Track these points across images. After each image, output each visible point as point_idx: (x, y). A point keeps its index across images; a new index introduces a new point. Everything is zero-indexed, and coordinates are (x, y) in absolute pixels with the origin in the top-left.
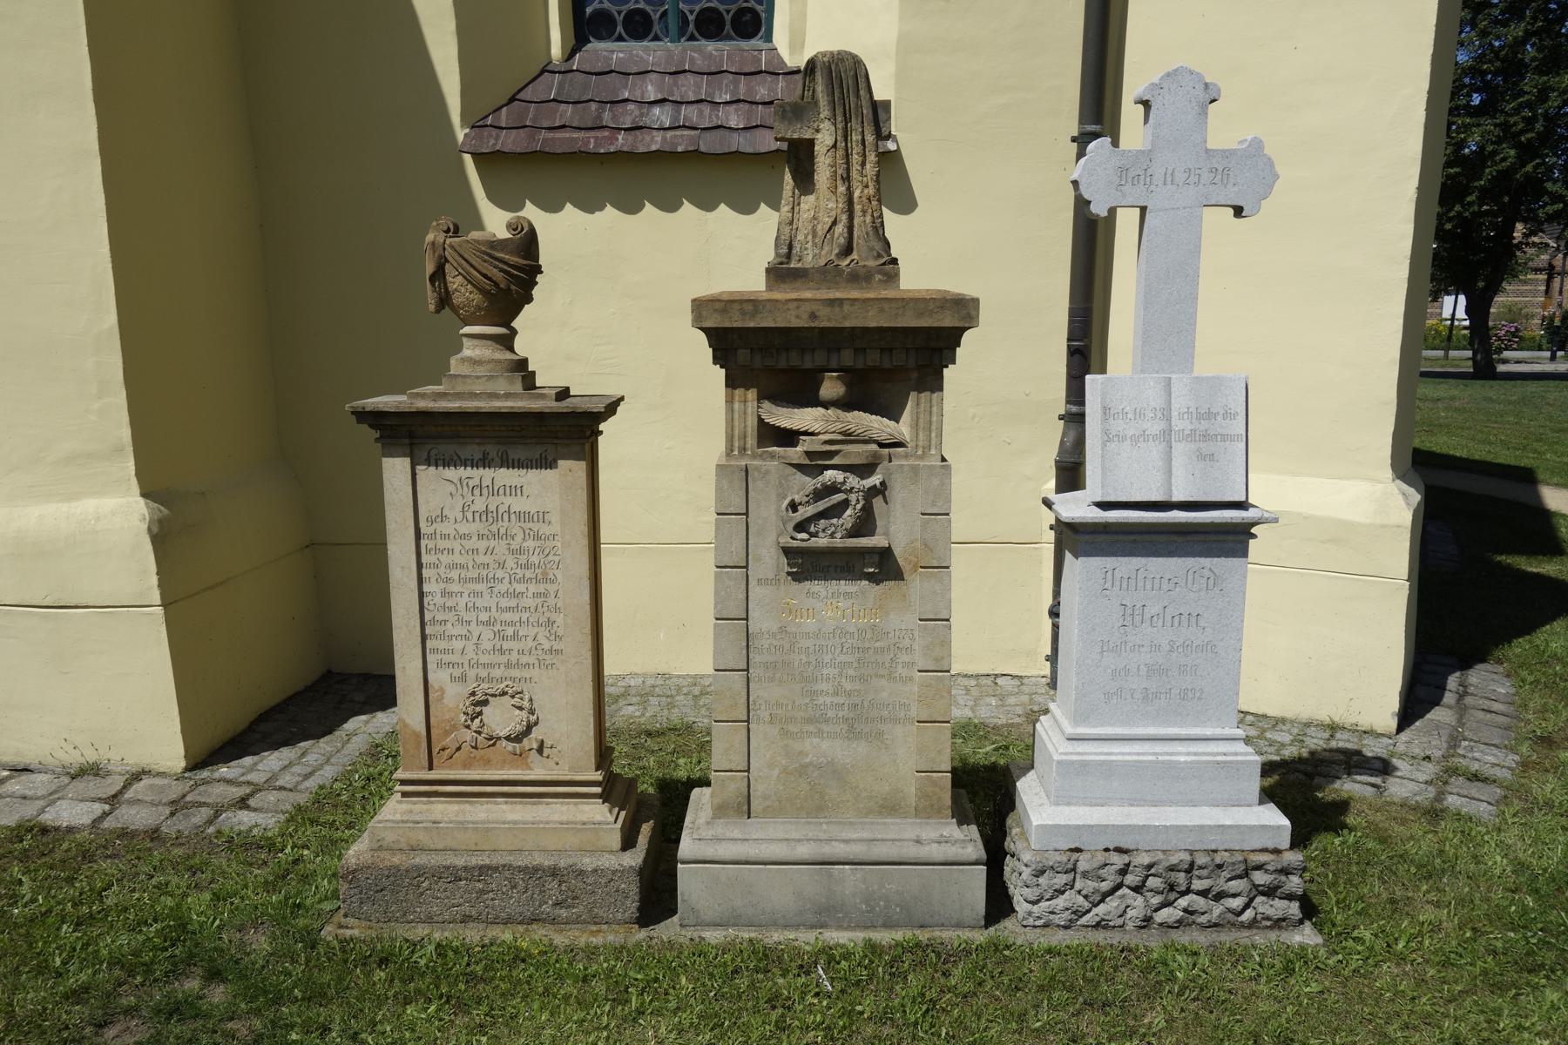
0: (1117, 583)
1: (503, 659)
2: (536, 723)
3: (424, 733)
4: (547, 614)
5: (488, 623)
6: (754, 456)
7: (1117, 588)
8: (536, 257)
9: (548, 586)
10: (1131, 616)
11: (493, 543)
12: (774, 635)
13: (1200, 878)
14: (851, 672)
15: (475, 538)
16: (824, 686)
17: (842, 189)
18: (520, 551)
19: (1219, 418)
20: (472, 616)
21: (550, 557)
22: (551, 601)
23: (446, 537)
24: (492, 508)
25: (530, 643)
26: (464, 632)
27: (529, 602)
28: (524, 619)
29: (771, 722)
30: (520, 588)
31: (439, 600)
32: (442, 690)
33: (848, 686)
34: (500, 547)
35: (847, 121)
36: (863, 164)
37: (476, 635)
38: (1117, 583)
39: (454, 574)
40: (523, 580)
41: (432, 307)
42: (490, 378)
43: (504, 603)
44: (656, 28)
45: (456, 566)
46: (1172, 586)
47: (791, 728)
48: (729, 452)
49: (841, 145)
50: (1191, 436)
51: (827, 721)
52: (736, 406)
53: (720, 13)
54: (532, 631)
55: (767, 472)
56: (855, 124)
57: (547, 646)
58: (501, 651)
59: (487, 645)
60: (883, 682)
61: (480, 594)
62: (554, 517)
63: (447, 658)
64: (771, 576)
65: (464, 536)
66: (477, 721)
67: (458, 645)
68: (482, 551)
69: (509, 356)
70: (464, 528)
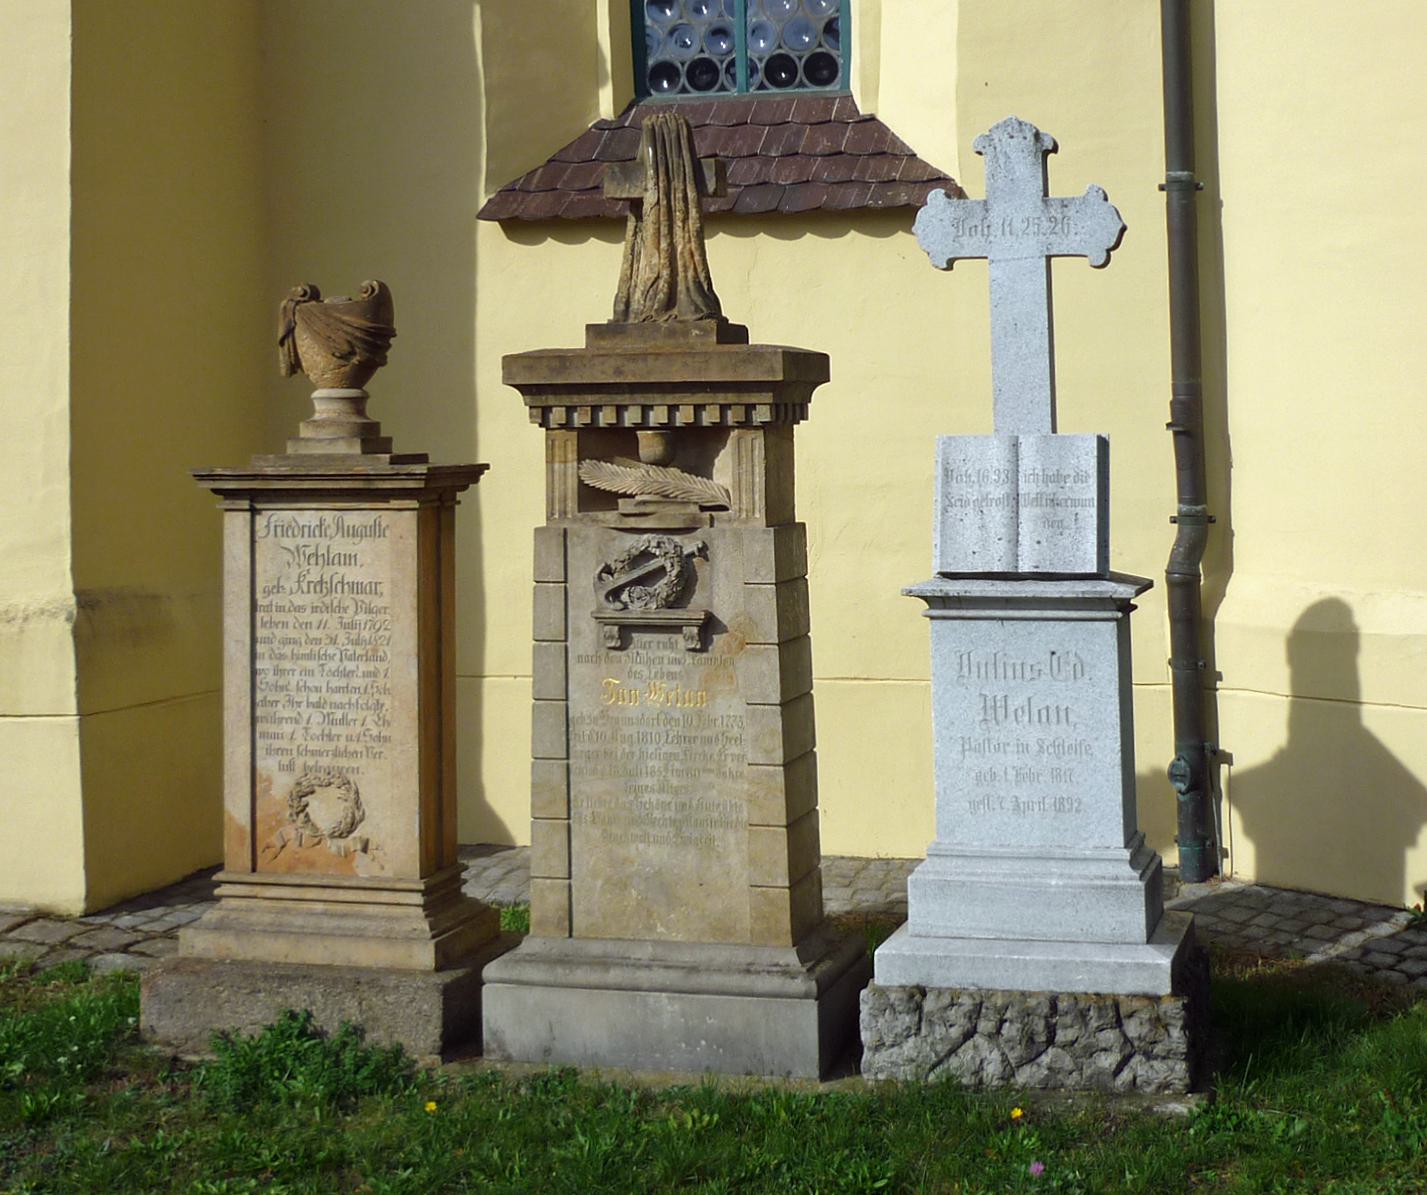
0: (974, 669)
1: (331, 746)
2: (361, 820)
3: (248, 828)
4: (376, 696)
5: (318, 705)
6: (575, 520)
7: (974, 675)
8: (390, 321)
9: (378, 664)
10: (994, 710)
11: (326, 616)
12: (595, 721)
13: (1066, 1027)
14: (677, 765)
15: (309, 610)
16: (648, 781)
17: (664, 245)
18: (352, 625)
19: (1070, 481)
20: (302, 697)
21: (381, 633)
22: (381, 681)
23: (280, 609)
24: (326, 578)
25: (358, 729)
26: (294, 715)
27: (357, 682)
28: (353, 701)
29: (594, 822)
30: (350, 666)
31: (270, 678)
32: (269, 780)
33: (675, 782)
34: (333, 620)
35: (669, 181)
36: (685, 220)
37: (305, 717)
38: (974, 669)
39: (287, 650)
40: (353, 657)
41: (283, 371)
42: (332, 441)
43: (336, 682)
44: (723, 77)
45: (287, 641)
46: (1036, 674)
47: (616, 830)
48: (550, 516)
49: (664, 202)
50: (1037, 500)
51: (653, 823)
52: (556, 466)
53: (688, 72)
54: (361, 714)
55: (587, 537)
56: (677, 184)
57: (375, 732)
58: (330, 737)
59: (316, 730)
60: (712, 777)
61: (311, 673)
62: (385, 588)
63: (277, 744)
64: (591, 652)
65: (300, 609)
66: (302, 815)
67: (287, 728)
68: (315, 624)
69: (360, 420)
70: (298, 600)
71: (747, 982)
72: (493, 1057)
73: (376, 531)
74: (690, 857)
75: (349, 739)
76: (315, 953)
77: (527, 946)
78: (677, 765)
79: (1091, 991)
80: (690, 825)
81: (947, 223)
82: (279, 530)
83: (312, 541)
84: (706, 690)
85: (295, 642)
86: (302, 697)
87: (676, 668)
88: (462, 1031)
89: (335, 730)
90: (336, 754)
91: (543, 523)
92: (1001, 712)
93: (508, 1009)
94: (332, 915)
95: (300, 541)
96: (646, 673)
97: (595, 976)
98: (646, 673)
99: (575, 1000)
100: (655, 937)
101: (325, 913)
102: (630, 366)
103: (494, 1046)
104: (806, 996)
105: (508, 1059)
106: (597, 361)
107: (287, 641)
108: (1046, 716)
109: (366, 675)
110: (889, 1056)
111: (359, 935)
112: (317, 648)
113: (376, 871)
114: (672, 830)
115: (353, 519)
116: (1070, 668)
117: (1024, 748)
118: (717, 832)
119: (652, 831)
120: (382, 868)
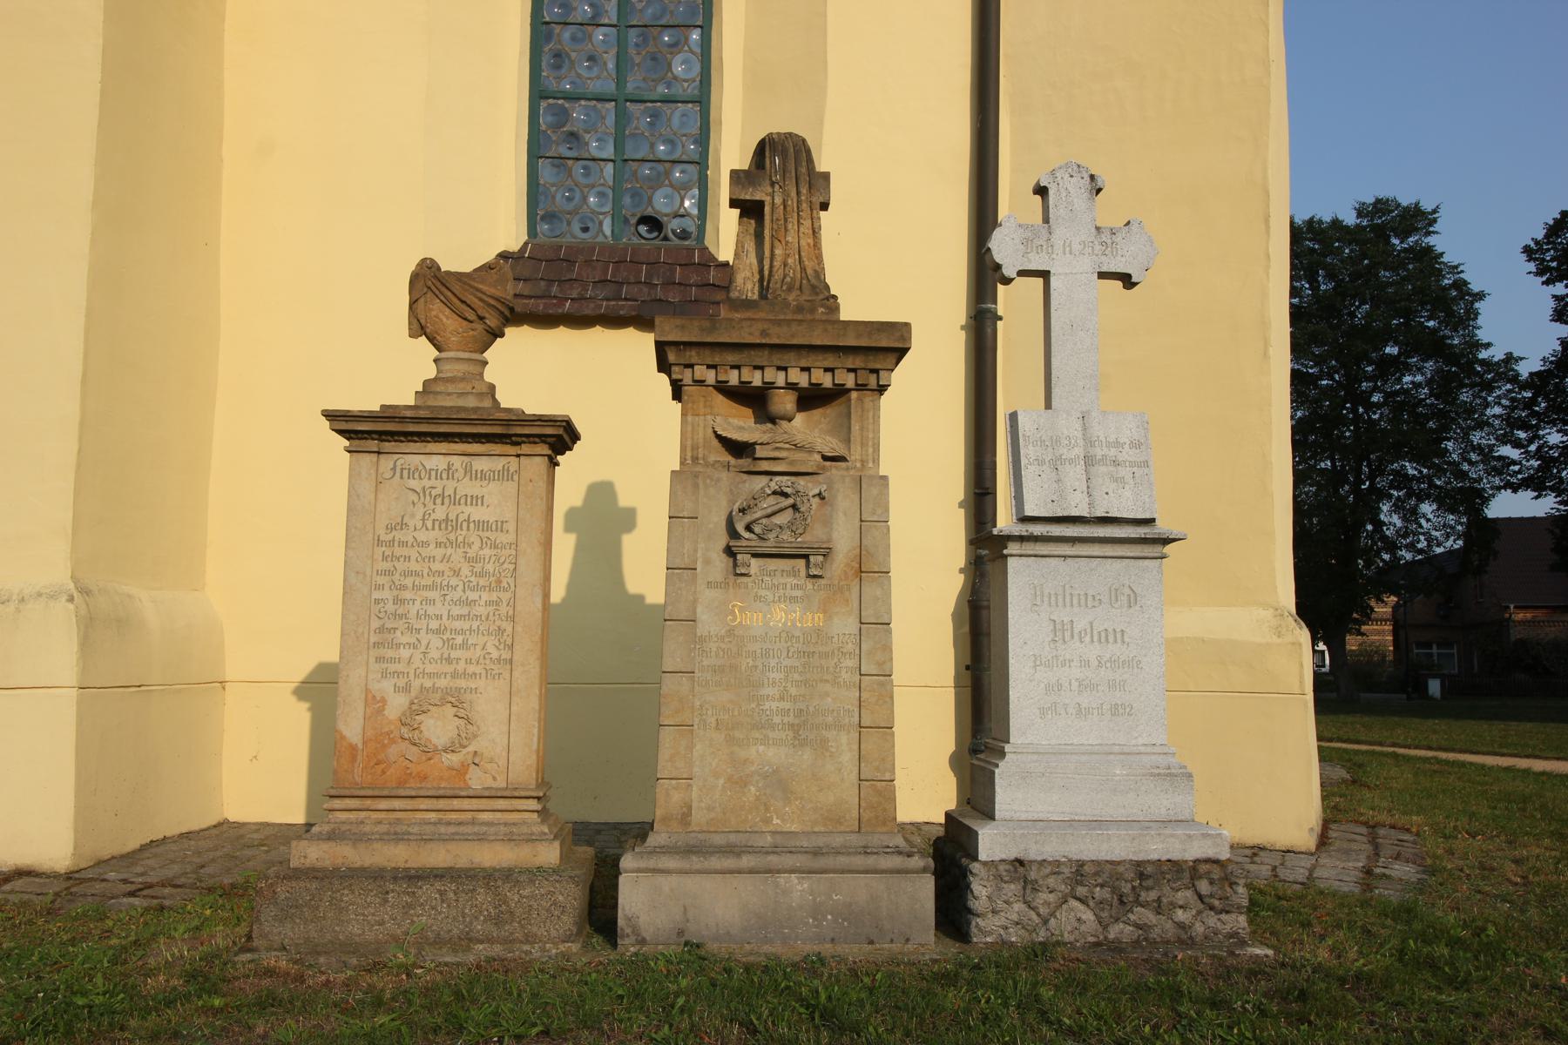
1: (449, 669)
5: (438, 632)
9: (501, 595)
11: (449, 551)
14: (796, 676)
15: (433, 546)
16: (769, 691)
18: (476, 560)
20: (422, 624)
23: (403, 544)
24: (452, 516)
26: (413, 640)
27: (480, 610)
29: (717, 728)
30: (473, 596)
33: (793, 691)
34: (457, 556)
37: (424, 643)
39: (408, 581)
40: (477, 588)
43: (456, 611)
45: (406, 574)
47: (737, 734)
48: (682, 463)
54: (481, 640)
55: (718, 480)
57: (495, 654)
58: (449, 660)
59: (434, 654)
60: (828, 687)
65: (425, 544)
68: (438, 558)
70: (422, 536)
71: (871, 861)
72: (627, 941)
73: (505, 475)
74: (807, 755)
75: (469, 661)
76: (438, 856)
77: (653, 840)
78: (796, 676)
79: (1164, 858)
80: (804, 730)
81: (1017, 241)
82: (405, 473)
83: (439, 483)
84: (825, 612)
85: (417, 574)
86: (422, 624)
87: (799, 593)
88: (600, 915)
89: (454, 654)
90: (455, 675)
91: (677, 468)
92: (1068, 634)
93: (643, 898)
94: (449, 823)
95: (426, 483)
96: (770, 597)
97: (729, 863)
98: (770, 597)
99: (710, 884)
100: (771, 828)
101: (439, 822)
102: (774, 330)
103: (628, 931)
104: (924, 870)
105: (643, 942)
106: (744, 324)
107: (406, 574)
108: (1105, 637)
109: (489, 603)
110: (998, 917)
111: (481, 838)
112: (439, 580)
113: (490, 783)
114: (791, 734)
115: (481, 464)
116: (1125, 598)
117: (1085, 663)
118: (831, 734)
119: (771, 735)
120: (495, 779)
